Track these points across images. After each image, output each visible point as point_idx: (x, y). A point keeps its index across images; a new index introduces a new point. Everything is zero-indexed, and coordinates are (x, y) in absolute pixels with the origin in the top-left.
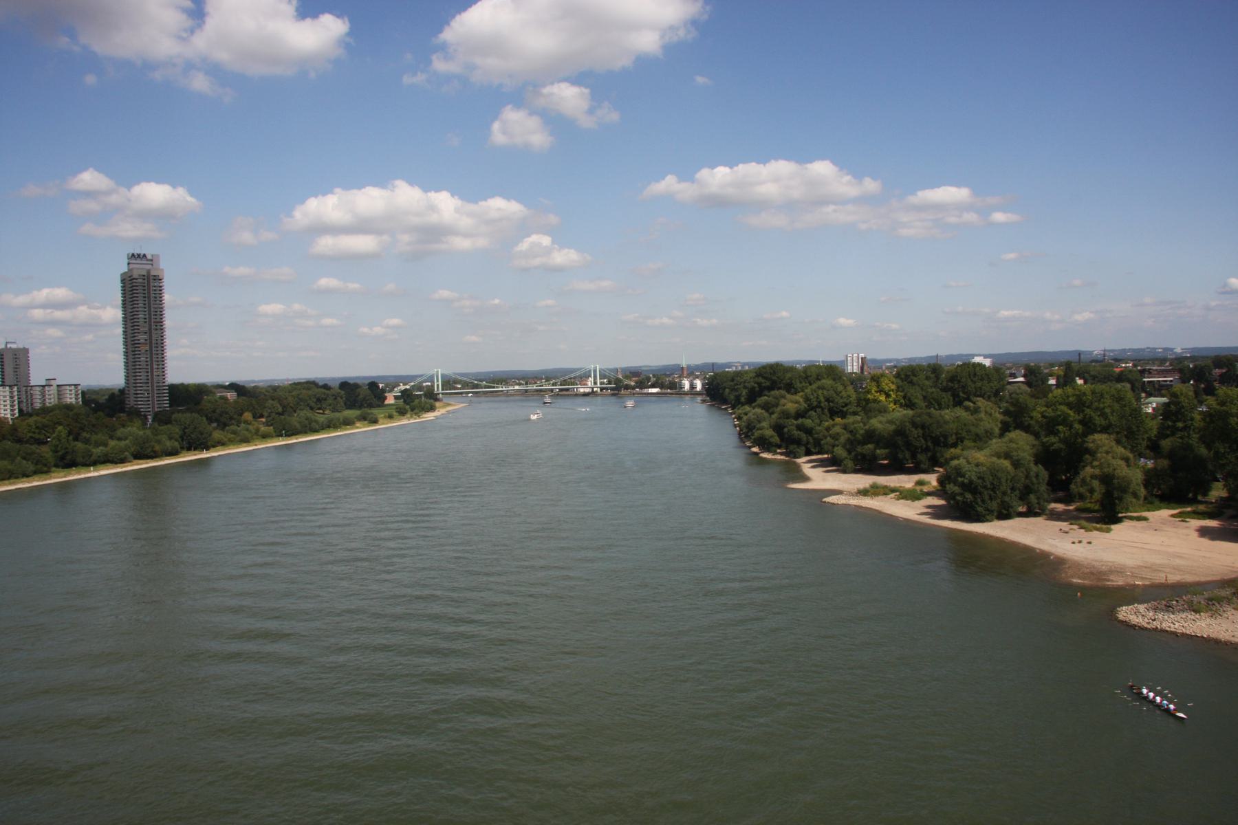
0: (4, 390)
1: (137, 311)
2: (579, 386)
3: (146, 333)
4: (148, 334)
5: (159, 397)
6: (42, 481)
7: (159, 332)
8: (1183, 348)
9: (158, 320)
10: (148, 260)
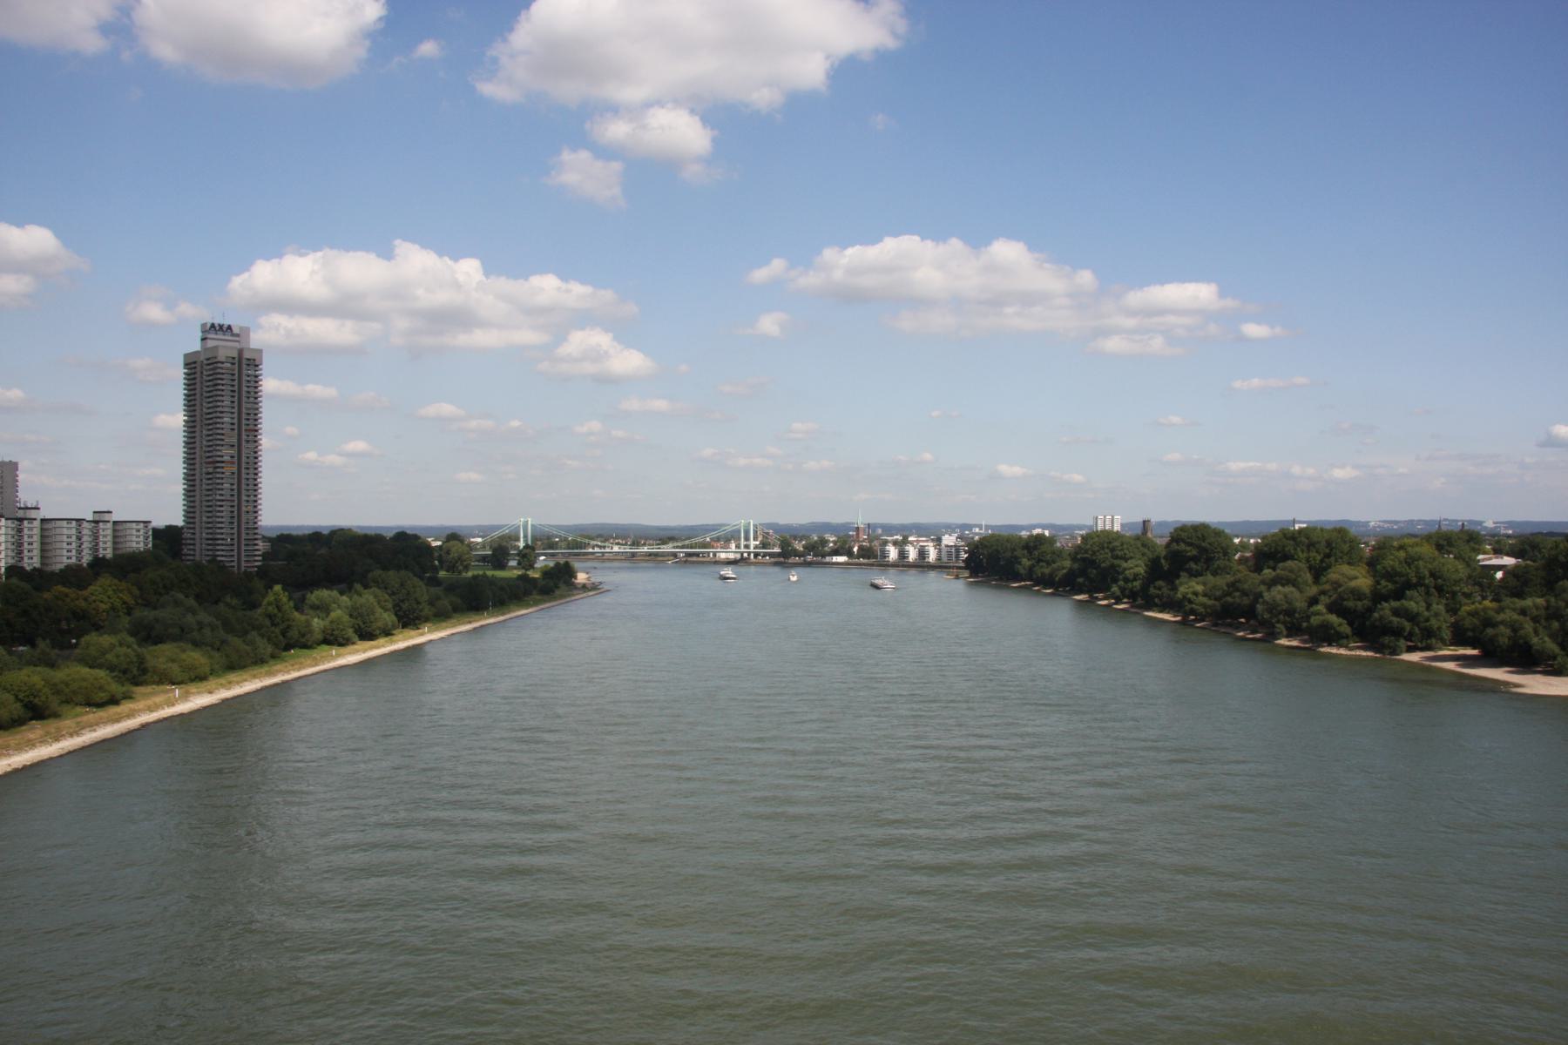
0: (69, 526)
1: (222, 412)
2: (719, 550)
3: (233, 446)
4: (236, 448)
5: (247, 545)
6: (299, 670)
7: (251, 445)
8: (1495, 521)
9: (251, 427)
10: (233, 335)
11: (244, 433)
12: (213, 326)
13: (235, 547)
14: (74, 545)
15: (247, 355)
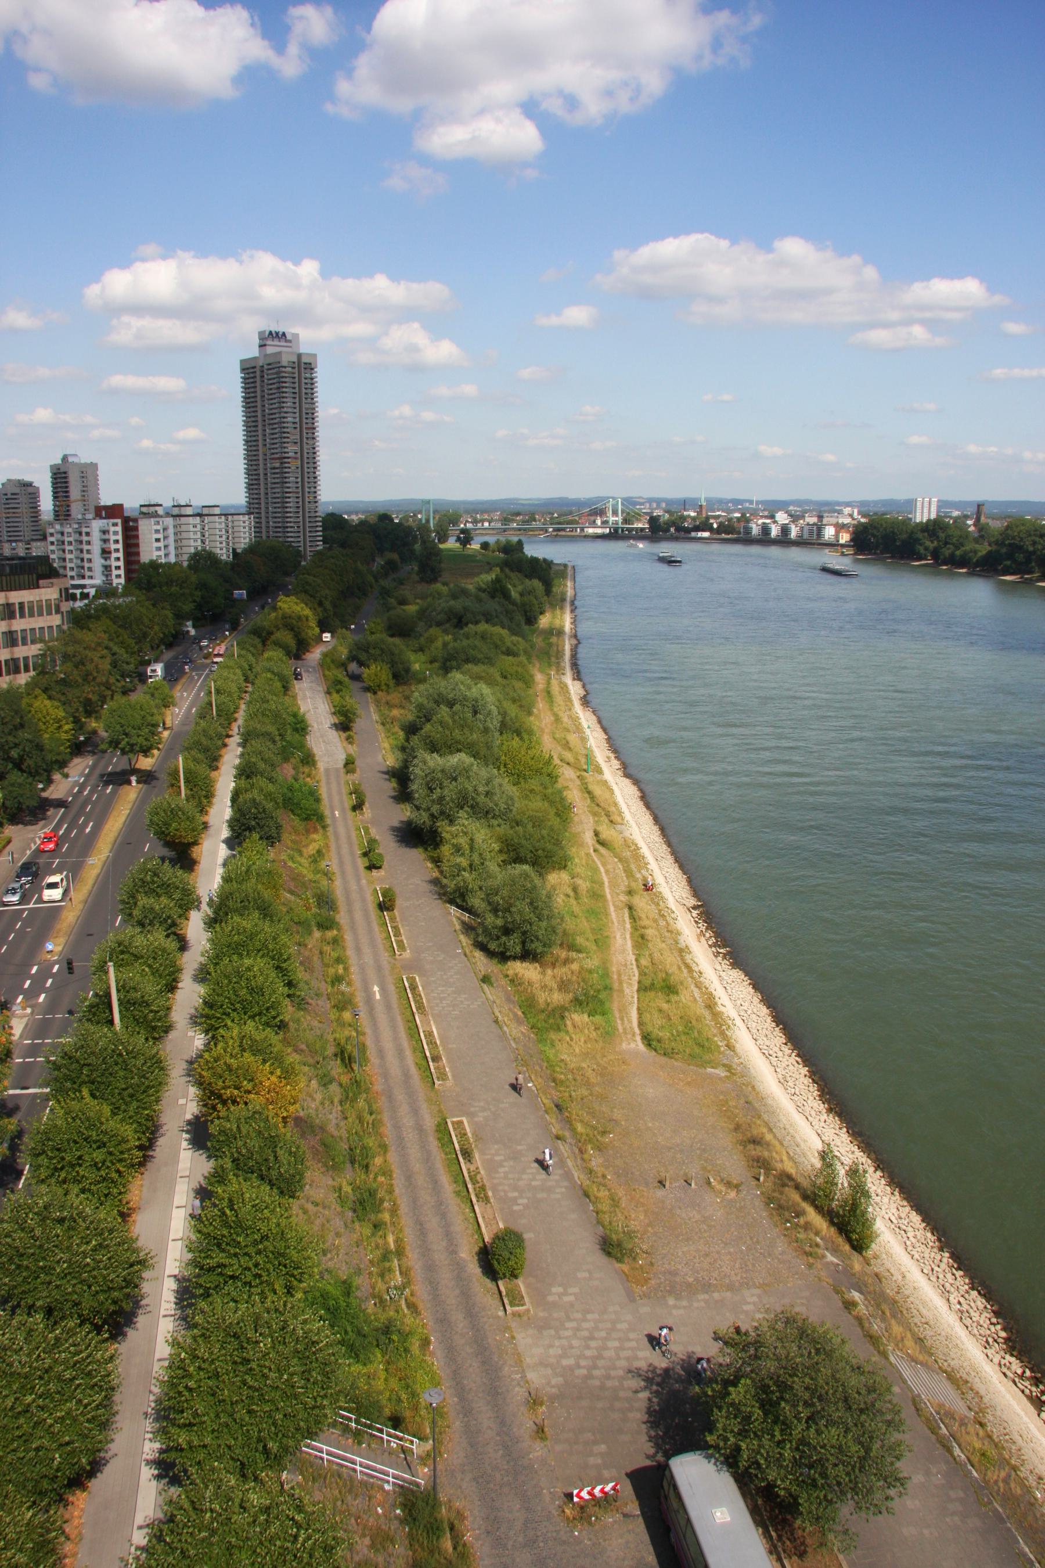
7: (310, 442)
9: (310, 425)
10: (286, 341)
11: (305, 431)
12: (271, 333)
13: (301, 534)
14: (224, 537)
15: (304, 360)
